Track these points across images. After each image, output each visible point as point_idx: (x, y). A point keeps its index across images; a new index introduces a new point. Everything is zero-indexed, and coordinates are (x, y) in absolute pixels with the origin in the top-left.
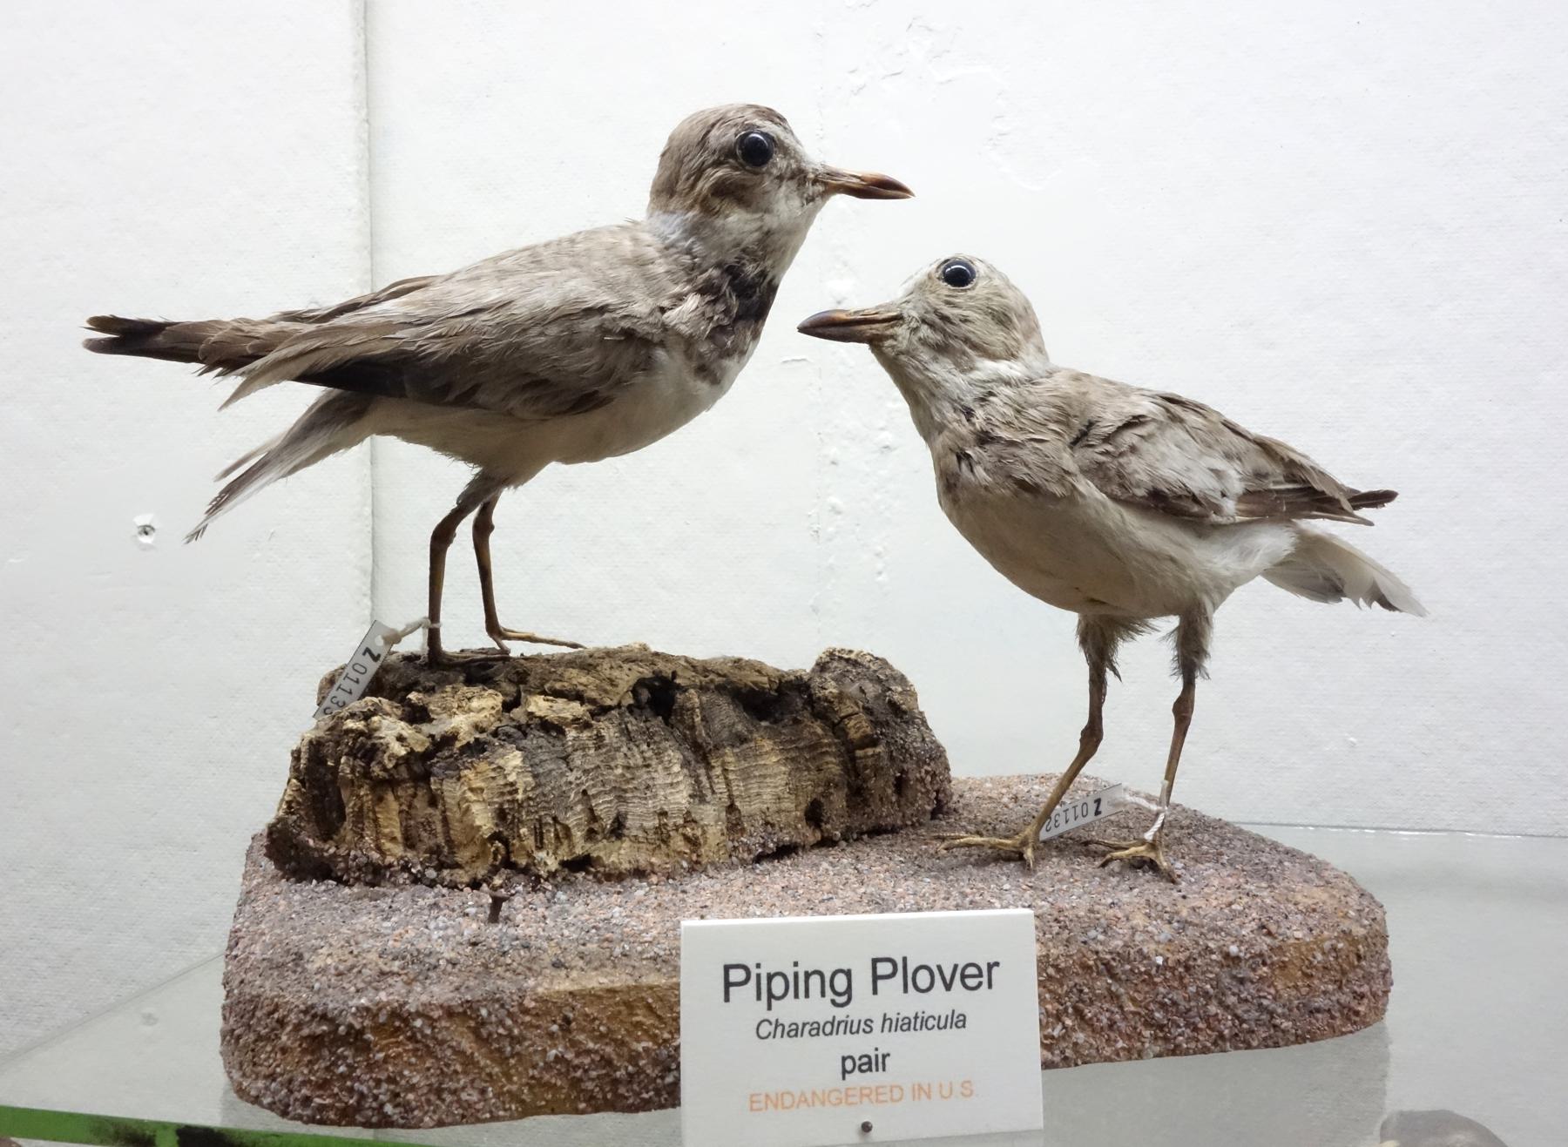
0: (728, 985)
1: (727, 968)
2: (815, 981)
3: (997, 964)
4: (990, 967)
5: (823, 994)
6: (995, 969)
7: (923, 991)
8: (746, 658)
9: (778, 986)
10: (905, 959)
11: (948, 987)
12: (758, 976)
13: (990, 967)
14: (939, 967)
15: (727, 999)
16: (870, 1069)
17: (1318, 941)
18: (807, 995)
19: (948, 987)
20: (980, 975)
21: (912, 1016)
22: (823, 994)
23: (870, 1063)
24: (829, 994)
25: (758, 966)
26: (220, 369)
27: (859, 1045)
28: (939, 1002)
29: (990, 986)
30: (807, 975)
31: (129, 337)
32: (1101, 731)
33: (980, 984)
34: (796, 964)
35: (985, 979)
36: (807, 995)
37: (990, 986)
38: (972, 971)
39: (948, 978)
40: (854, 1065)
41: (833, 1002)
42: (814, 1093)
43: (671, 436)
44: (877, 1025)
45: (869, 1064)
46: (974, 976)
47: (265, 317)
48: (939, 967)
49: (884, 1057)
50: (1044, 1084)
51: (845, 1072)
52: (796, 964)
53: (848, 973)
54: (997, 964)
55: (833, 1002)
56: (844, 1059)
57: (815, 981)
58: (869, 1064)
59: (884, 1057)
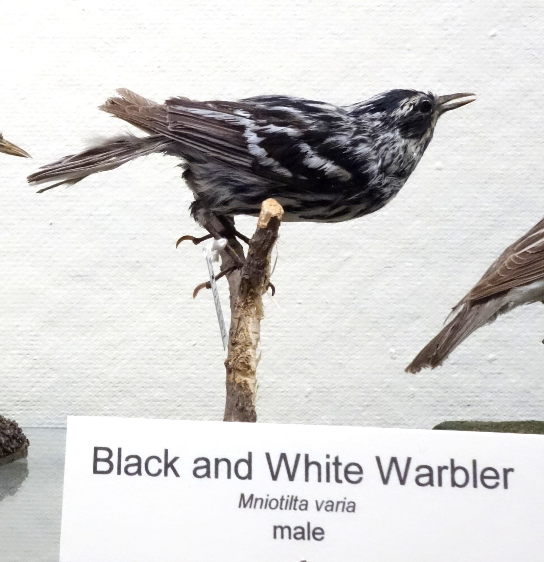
1: (96, 449)
3: (512, 470)
4: (506, 471)
6: (510, 474)
7: (244, 478)
10: (120, 450)
13: (506, 471)
16: (303, 538)
21: (279, 499)
23: (303, 533)
26: (113, 115)
27: (293, 518)
29: (506, 486)
32: (199, 243)
33: (497, 484)
35: (501, 481)
36: (217, 476)
37: (506, 486)
44: (312, 506)
47: (202, 99)
52: (328, 456)
54: (512, 470)
57: (223, 466)
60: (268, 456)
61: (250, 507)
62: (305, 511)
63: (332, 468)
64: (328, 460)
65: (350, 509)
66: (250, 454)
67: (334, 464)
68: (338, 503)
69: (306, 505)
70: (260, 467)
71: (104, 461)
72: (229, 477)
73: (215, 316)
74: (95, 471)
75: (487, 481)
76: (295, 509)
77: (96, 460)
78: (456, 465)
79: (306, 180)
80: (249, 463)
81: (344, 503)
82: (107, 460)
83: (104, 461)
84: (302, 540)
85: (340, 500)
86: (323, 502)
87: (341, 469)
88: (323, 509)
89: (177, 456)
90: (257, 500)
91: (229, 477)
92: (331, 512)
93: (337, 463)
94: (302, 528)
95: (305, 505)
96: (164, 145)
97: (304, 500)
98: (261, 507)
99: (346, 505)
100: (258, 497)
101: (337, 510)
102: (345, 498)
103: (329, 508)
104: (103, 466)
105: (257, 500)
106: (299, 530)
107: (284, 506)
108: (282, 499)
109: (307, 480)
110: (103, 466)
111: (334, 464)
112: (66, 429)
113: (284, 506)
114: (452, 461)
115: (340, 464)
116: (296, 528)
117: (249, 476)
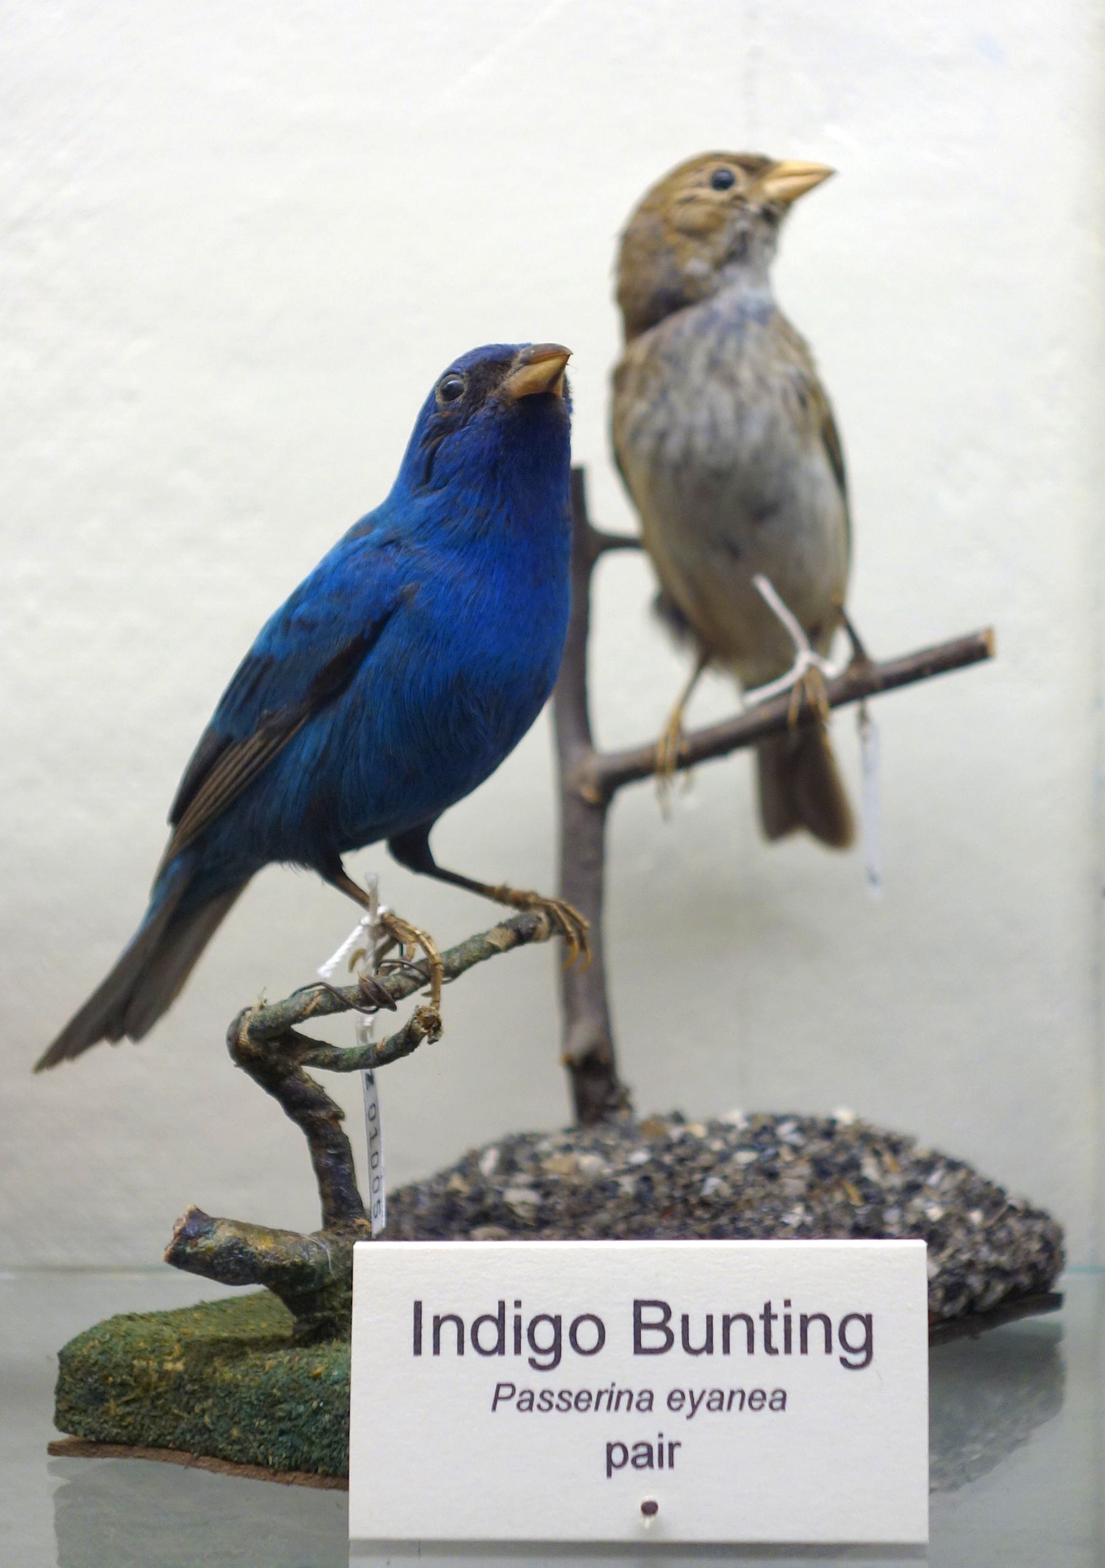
0: (497, 1398)
1: (638, 1305)
5: (828, 1349)
9: (488, 1335)
12: (788, 1319)
16: (650, 1463)
22: (828, 1349)
23: (649, 1454)
24: (526, 1350)
25: (787, 1303)
27: (632, 1427)
30: (805, 1320)
31: (971, 653)
36: (804, 1350)
38: (652, 1315)
40: (618, 1454)
41: (532, 1362)
45: (655, 1456)
46: (854, 1342)
49: (672, 1446)
50: (931, 1509)
51: (610, 1463)
53: (867, 1321)
55: (532, 1362)
56: (610, 1448)
57: (816, 1329)
58: (655, 1456)
60: (418, 1306)
62: (781, 1412)
64: (788, 1311)
65: (644, 1405)
67: (761, 1317)
68: (600, 1394)
69: (670, 1398)
72: (461, 1351)
74: (639, 1349)
77: (639, 1326)
81: (612, 1393)
82: (662, 1326)
83: (426, 1330)
84: (647, 1469)
85: (603, 1389)
86: (704, 1392)
88: (703, 1406)
89: (766, 1301)
91: (461, 1351)
92: (718, 1412)
93: (768, 1316)
94: (650, 1448)
95: (674, 1399)
96: (366, 636)
97: (646, 1391)
98: (609, 1408)
99: (636, 1398)
100: (623, 1388)
101: (729, 1408)
102: (613, 1385)
103: (714, 1405)
104: (653, 1339)
105: (620, 1394)
110: (653, 1339)
111: (761, 1317)
115: (775, 1317)
116: (636, 1447)
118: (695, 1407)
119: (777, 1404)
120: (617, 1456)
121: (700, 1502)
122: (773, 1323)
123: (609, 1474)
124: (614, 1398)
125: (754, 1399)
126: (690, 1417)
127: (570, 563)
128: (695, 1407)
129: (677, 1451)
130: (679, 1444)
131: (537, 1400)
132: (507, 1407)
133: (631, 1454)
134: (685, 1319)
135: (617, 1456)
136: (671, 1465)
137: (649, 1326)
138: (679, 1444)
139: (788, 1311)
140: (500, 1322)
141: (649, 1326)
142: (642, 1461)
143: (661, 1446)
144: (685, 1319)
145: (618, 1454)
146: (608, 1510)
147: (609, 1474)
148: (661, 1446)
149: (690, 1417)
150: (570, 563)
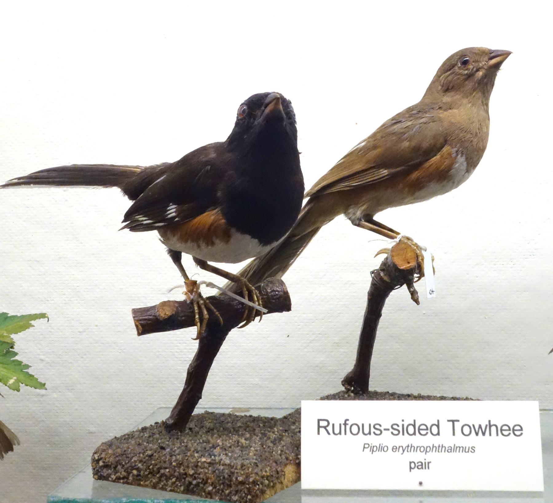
0: (364, 448)
2: (366, 431)
7: (436, 435)
8: (416, 241)
11: (477, 434)
14: (473, 426)
15: (319, 433)
16: (422, 468)
17: (232, 435)
18: (490, 435)
19: (477, 434)
20: (427, 429)
23: (422, 465)
27: (418, 457)
28: (473, 440)
33: (427, 433)
34: (403, 421)
38: (505, 428)
39: (483, 430)
40: (412, 466)
42: (484, 434)
43: (374, 347)
45: (422, 466)
46: (516, 430)
48: (473, 426)
49: (429, 463)
51: (411, 468)
52: (403, 421)
56: (410, 463)
57: (366, 431)
58: (422, 466)
59: (429, 463)
61: (408, 451)
63: (343, 427)
64: (403, 423)
66: (438, 421)
68: (417, 447)
69: (393, 449)
70: (446, 427)
71: (323, 425)
73: (182, 381)
75: (421, 432)
76: (438, 452)
78: (455, 423)
79: (220, 323)
80: (438, 426)
83: (323, 425)
84: (421, 470)
87: (348, 427)
88: (406, 451)
90: (457, 447)
91: (497, 435)
94: (422, 463)
99: (447, 449)
106: (420, 464)
107: (440, 450)
108: (439, 447)
109: (454, 434)
112: (541, 410)
113: (440, 450)
114: (490, 421)
116: (418, 463)
117: (438, 434)
118: (404, 451)
119: (449, 451)
120: (413, 465)
121: (433, 480)
122: (347, 426)
123: (410, 471)
124: (410, 448)
125: (464, 450)
126: (402, 454)
127: (363, 208)
128: (404, 451)
129: (430, 464)
130: (430, 462)
131: (470, 449)
132: (367, 450)
133: (417, 465)
134: (333, 425)
135: (413, 465)
136: (428, 468)
137: (322, 427)
138: (430, 462)
139: (403, 423)
140: (414, 426)
141: (322, 427)
142: (420, 467)
143: (425, 463)
144: (333, 425)
145: (412, 466)
146: (409, 481)
147: (410, 471)
148: (425, 463)
149: (402, 454)
150: (363, 208)
